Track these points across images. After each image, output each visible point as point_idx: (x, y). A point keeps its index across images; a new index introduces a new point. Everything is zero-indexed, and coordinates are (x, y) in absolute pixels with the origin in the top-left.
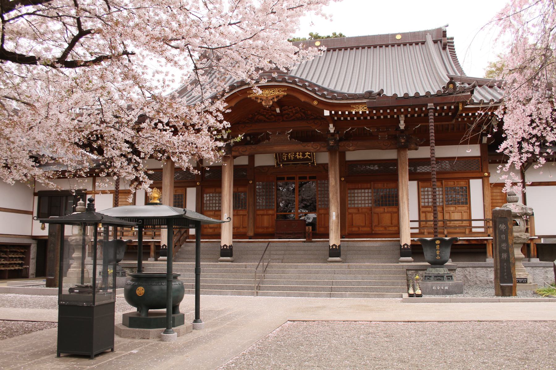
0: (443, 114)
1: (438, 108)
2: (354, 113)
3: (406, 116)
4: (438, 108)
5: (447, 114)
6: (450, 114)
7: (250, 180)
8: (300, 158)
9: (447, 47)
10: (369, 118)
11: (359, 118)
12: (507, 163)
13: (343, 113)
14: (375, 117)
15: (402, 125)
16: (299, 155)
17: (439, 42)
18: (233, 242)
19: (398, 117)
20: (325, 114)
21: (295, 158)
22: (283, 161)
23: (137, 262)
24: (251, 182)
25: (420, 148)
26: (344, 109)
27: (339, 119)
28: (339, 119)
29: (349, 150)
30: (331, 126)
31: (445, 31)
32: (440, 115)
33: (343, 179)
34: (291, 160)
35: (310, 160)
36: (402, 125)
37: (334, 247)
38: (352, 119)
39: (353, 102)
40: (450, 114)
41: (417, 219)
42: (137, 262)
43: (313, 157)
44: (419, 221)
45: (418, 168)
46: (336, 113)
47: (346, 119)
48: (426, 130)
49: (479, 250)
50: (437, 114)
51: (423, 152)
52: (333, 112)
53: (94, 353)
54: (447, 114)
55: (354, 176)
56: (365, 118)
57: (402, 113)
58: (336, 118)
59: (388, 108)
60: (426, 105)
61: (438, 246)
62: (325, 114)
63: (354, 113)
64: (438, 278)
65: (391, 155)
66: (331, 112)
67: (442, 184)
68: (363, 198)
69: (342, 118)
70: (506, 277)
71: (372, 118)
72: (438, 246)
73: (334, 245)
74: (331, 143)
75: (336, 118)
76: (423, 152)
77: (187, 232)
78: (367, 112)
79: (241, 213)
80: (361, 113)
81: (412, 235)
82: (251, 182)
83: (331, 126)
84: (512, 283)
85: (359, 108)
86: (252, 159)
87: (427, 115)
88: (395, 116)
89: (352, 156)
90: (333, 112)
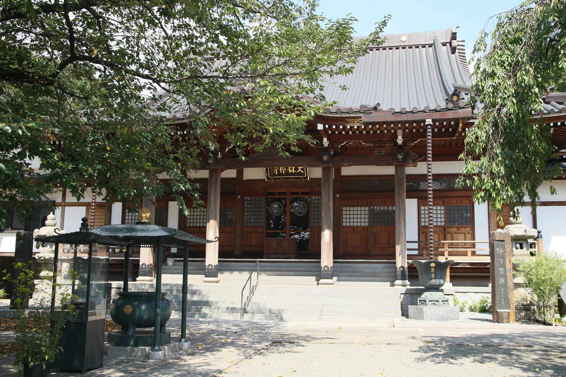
0: (443, 130)
1: (437, 124)
2: (348, 127)
3: (404, 131)
4: (437, 124)
5: (447, 130)
6: (450, 130)
7: (238, 195)
8: (292, 172)
9: (457, 51)
10: (364, 132)
11: (354, 132)
12: (63, 329)
13: (337, 127)
14: (371, 132)
15: (400, 140)
16: (291, 169)
17: (448, 44)
18: (219, 261)
19: (395, 131)
20: (318, 129)
21: (287, 172)
22: (275, 175)
23: (123, 282)
24: (239, 197)
25: (419, 164)
26: (338, 123)
27: (333, 133)
28: (333, 133)
29: (344, 166)
30: (325, 140)
31: (455, 33)
32: (440, 130)
33: (338, 196)
34: (282, 174)
35: (303, 174)
36: (400, 140)
37: (326, 268)
38: (347, 133)
39: (348, 115)
40: (450, 130)
41: (417, 240)
42: (123, 282)
43: (306, 171)
44: (419, 242)
45: (421, 183)
46: (330, 127)
47: (340, 133)
48: (424, 146)
49: (483, 274)
50: (436, 130)
51: (420, 168)
52: (327, 126)
53: (85, 368)
54: (447, 130)
55: (352, 192)
56: (361, 132)
57: (400, 128)
58: (330, 132)
59: (385, 123)
60: (424, 121)
61: (433, 269)
62: (318, 129)
63: (348, 127)
64: (433, 302)
65: (389, 170)
66: (324, 126)
67: (444, 202)
68: (357, 217)
69: (337, 132)
70: (503, 303)
71: (368, 132)
72: (433, 269)
73: (326, 266)
74: (325, 158)
75: (330, 132)
76: (420, 168)
77: (169, 249)
78: (363, 127)
79: (228, 229)
80: (356, 127)
81: (409, 257)
82: (239, 197)
83: (325, 140)
84: (510, 309)
85: (354, 122)
86: (240, 173)
87: (425, 130)
88: (393, 131)
89: (348, 171)
90: (327, 126)
